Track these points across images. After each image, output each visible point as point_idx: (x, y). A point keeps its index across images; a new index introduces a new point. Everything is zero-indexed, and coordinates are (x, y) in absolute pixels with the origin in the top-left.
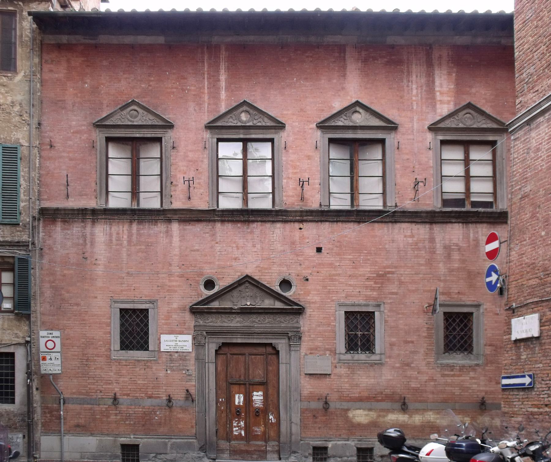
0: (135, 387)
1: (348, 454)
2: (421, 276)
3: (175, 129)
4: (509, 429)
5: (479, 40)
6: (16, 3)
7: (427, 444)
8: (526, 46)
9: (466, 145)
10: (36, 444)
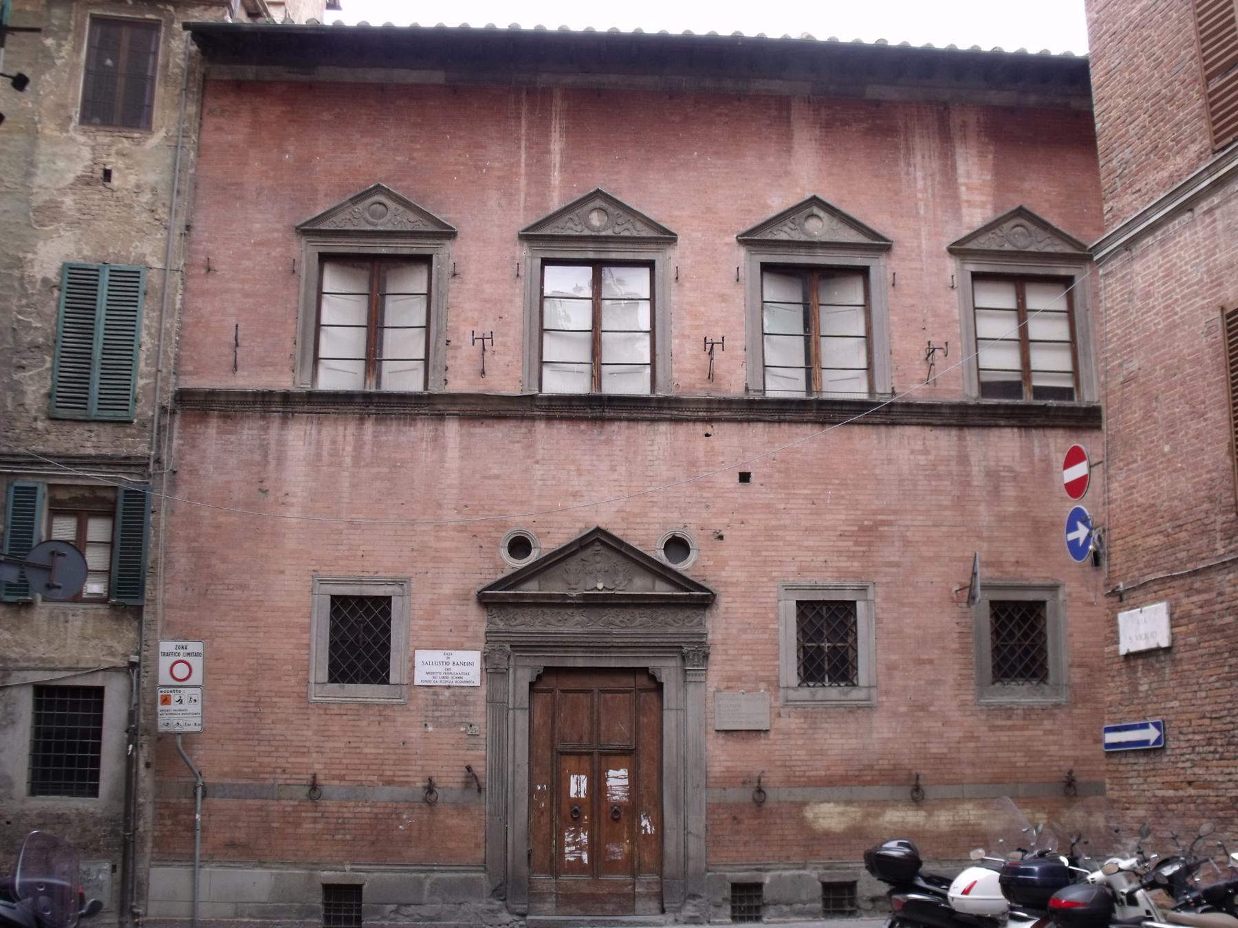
0: (357, 761)
1: (804, 897)
2: (945, 529)
3: (458, 239)
4: (1122, 833)
5: (1032, 99)
6: (161, 6)
7: (963, 870)
8: (1114, 114)
9: (1020, 282)
10: (140, 884)
